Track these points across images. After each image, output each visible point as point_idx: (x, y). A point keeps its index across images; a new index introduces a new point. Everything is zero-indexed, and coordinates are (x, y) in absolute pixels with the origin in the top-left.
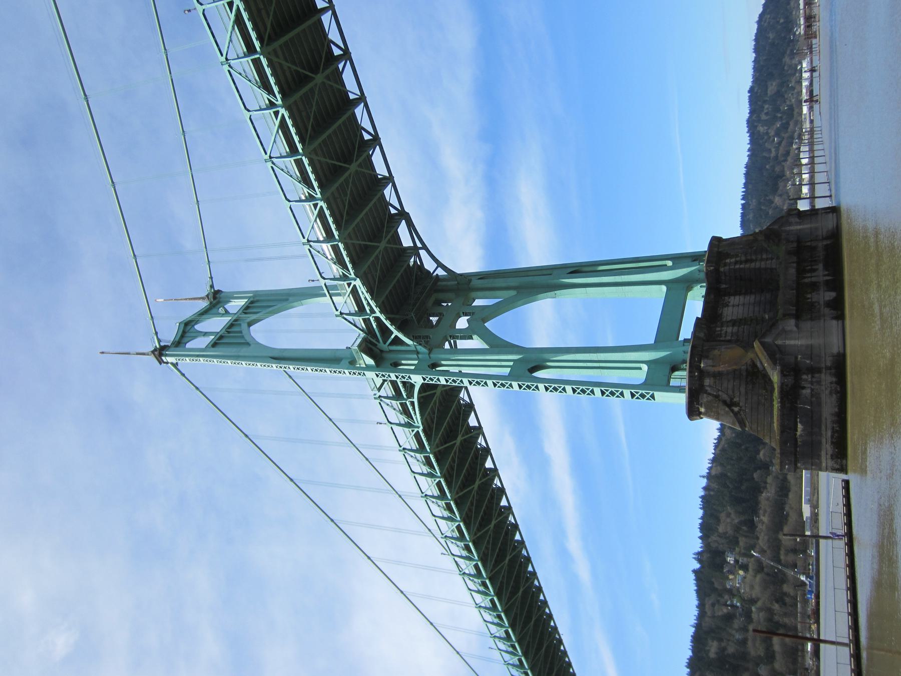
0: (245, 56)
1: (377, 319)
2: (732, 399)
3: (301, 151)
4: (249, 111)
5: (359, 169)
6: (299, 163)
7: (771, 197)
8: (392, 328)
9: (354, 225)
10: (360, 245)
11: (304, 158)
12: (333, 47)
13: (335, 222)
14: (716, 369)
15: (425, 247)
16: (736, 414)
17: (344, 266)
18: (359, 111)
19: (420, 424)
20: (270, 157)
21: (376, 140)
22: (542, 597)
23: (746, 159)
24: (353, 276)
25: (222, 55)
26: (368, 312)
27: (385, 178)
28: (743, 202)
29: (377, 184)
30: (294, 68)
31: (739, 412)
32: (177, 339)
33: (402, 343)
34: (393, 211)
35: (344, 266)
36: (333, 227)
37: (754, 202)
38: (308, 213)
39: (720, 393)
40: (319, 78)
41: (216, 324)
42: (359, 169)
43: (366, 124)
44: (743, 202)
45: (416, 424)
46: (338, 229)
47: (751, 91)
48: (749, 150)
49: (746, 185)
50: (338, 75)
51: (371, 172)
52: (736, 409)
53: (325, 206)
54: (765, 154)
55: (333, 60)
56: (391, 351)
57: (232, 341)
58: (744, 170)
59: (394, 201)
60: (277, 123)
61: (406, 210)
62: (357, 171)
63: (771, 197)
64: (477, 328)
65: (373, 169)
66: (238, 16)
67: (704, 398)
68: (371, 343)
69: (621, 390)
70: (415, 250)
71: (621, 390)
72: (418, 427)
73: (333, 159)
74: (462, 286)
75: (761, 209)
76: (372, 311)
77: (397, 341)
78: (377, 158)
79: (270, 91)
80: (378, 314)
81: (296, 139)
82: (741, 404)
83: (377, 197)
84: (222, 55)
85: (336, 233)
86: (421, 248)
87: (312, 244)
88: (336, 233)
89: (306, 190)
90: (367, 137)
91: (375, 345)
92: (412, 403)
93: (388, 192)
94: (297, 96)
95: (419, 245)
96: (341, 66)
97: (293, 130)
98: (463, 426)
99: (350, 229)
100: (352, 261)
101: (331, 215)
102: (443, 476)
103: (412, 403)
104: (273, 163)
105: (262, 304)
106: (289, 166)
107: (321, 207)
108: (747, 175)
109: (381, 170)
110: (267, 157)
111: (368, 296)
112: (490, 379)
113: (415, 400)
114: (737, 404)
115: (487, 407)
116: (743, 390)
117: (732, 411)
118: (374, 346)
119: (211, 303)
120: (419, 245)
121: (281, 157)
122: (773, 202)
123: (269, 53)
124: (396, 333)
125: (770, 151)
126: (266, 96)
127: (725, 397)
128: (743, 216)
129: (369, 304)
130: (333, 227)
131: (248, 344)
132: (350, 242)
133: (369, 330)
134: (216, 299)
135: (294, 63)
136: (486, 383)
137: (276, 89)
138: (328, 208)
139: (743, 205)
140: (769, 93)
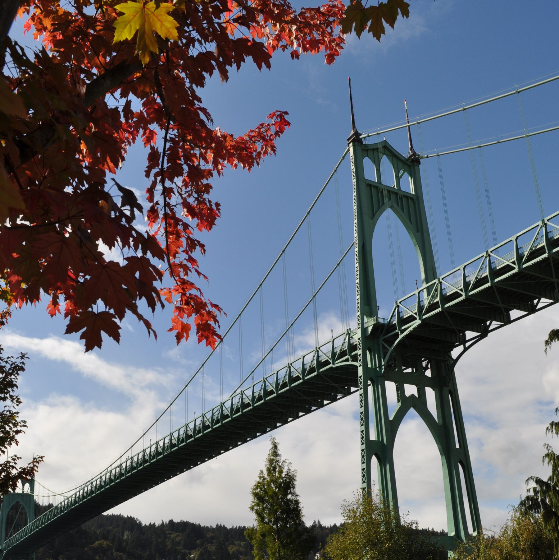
1: (397, 335)
15: (466, 349)
22: (326, 402)
26: (403, 328)
32: (370, 148)
41: (389, 178)
56: (379, 345)
57: (373, 199)
61: (489, 334)
64: (406, 403)
69: (366, 481)
70: (463, 341)
71: (366, 481)
74: (445, 384)
76: (403, 331)
86: (465, 346)
92: (347, 360)
95: (467, 345)
103: (347, 360)
105: (412, 211)
111: (411, 329)
112: (365, 409)
115: (349, 404)
119: (407, 160)
120: (467, 345)
131: (373, 215)
134: (412, 164)
136: (362, 406)
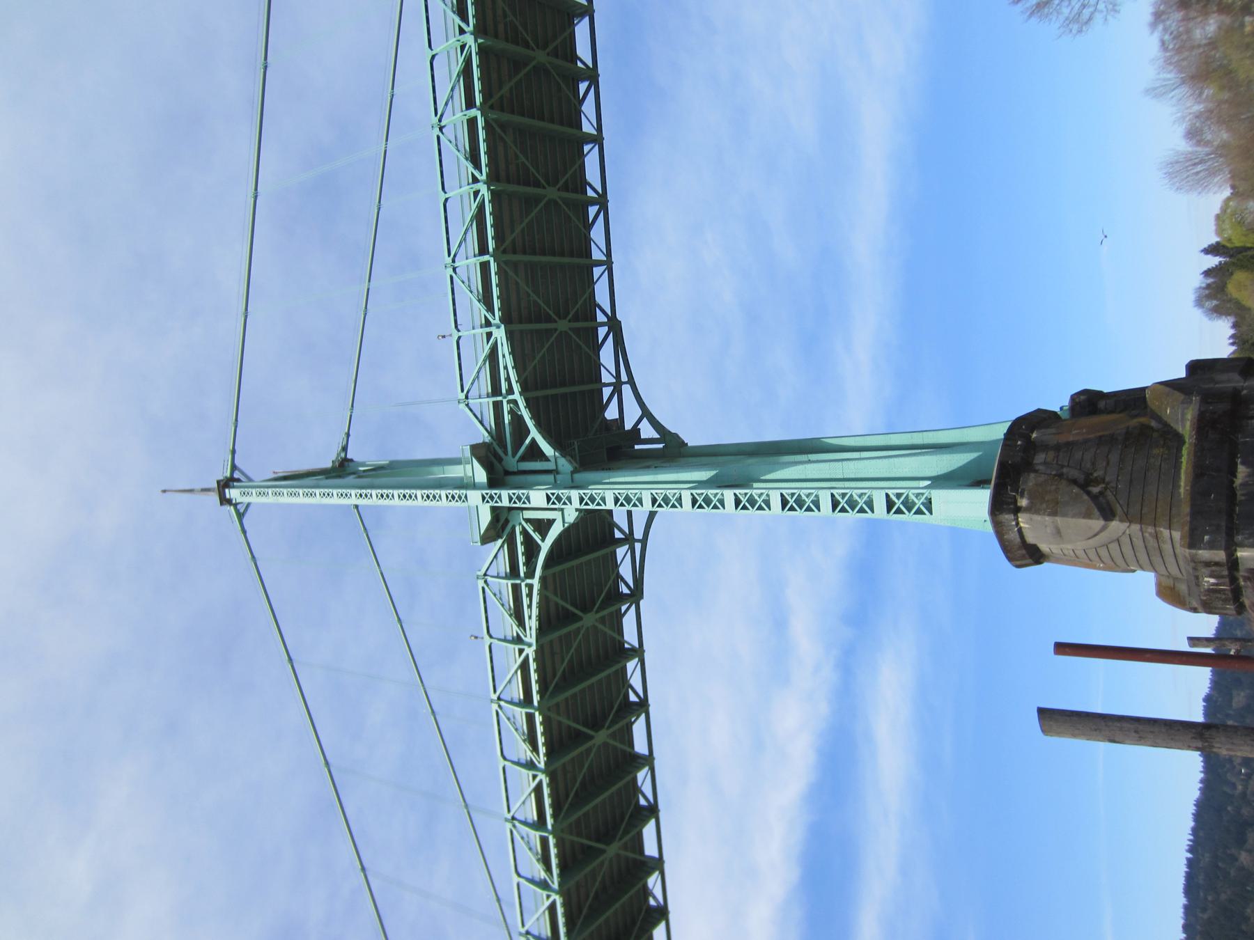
0: (506, 577)
2: (1088, 475)
3: (536, 703)
4: (491, 637)
5: (611, 742)
6: (530, 718)
7: (1233, 851)
8: (530, 423)
9: (593, 927)
10: (569, 727)
11: (537, 714)
12: (616, 531)
13: (553, 805)
14: (1063, 439)
16: (1094, 498)
17: (548, 869)
18: (631, 665)
19: (533, 641)
20: (499, 699)
21: (652, 811)
23: (1197, 794)
24: (497, 321)
25: (495, 691)
27: (633, 649)
28: (1189, 855)
29: (618, 653)
30: (534, 296)
31: (1101, 493)
33: (540, 455)
34: (643, 802)
35: (535, 749)
36: (549, 811)
37: (1207, 858)
38: (525, 782)
39: (1065, 470)
40: (589, 620)
42: (611, 742)
43: (636, 681)
44: (1189, 855)
45: (527, 640)
46: (554, 816)
47: (1207, 699)
48: (1201, 781)
49: (1195, 831)
50: (620, 616)
51: (615, 635)
52: (1095, 490)
53: (546, 781)
54: (1227, 789)
55: (616, 597)
58: (1192, 809)
59: (658, 892)
60: (520, 661)
62: (595, 627)
63: (1233, 851)
65: (631, 744)
66: (481, 208)
67: (1031, 481)
68: (496, 455)
72: (530, 645)
73: (566, 601)
75: (1217, 867)
76: (510, 391)
77: (534, 453)
78: (649, 831)
79: (490, 308)
80: (517, 396)
81: (535, 687)
82: (1107, 479)
83: (620, 784)
84: (495, 691)
85: (536, 698)
87: (502, 703)
88: (536, 698)
89: (515, 628)
90: (633, 698)
91: (500, 460)
92: (530, 587)
93: (642, 775)
94: (555, 635)
96: (624, 608)
97: (534, 677)
98: (626, 832)
99: (561, 698)
100: (560, 866)
101: (551, 795)
102: (540, 653)
104: (500, 706)
106: (518, 717)
107: (541, 782)
108: (1198, 817)
109: (650, 849)
110: (495, 697)
111: (509, 361)
113: (535, 582)
114: (1097, 482)
116: (1114, 457)
117: (1089, 493)
118: (501, 460)
121: (498, 577)
122: (1236, 860)
123: (549, 709)
124: (534, 434)
125: (1234, 786)
126: (484, 312)
127: (1074, 473)
128: (1189, 877)
129: (508, 379)
130: (549, 811)
132: (553, 715)
133: (498, 434)
135: (563, 598)
137: (497, 304)
138: (549, 785)
139: (1188, 860)
140: (1234, 705)
